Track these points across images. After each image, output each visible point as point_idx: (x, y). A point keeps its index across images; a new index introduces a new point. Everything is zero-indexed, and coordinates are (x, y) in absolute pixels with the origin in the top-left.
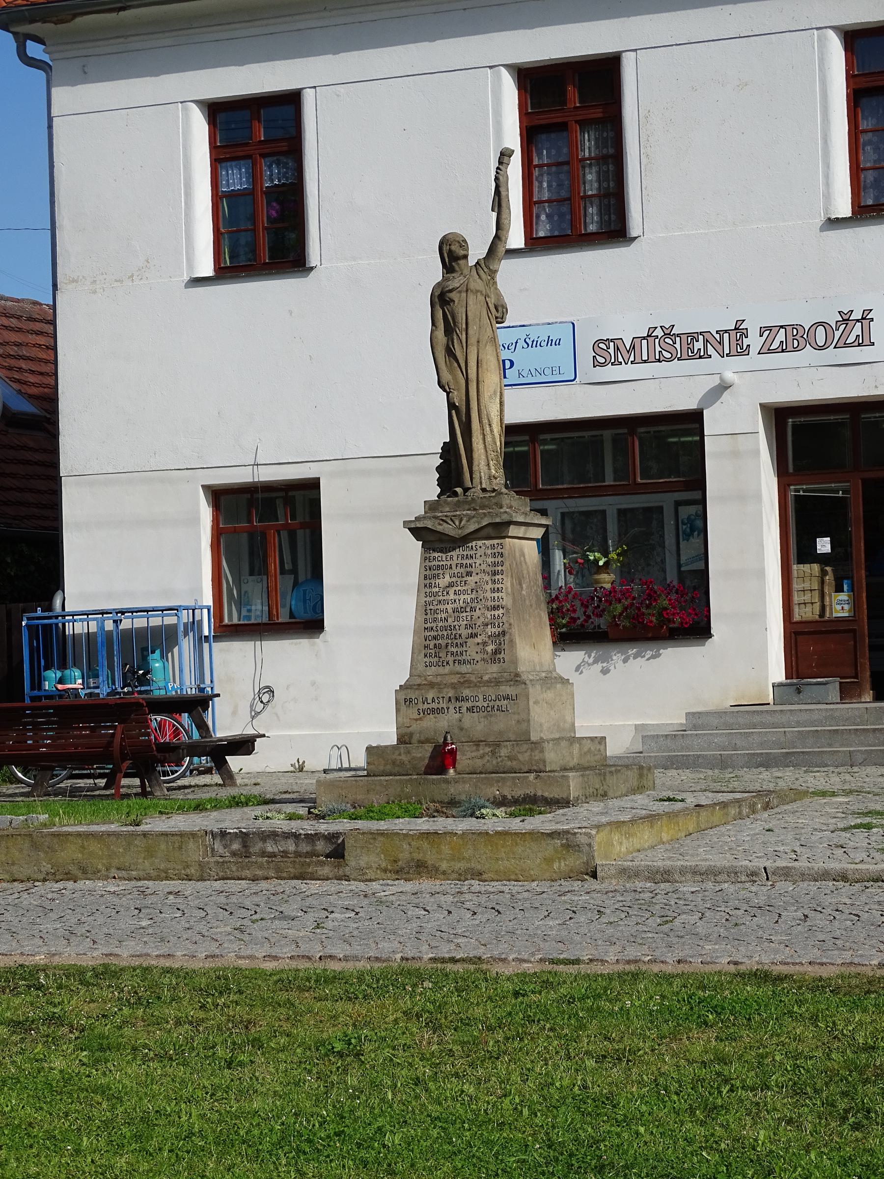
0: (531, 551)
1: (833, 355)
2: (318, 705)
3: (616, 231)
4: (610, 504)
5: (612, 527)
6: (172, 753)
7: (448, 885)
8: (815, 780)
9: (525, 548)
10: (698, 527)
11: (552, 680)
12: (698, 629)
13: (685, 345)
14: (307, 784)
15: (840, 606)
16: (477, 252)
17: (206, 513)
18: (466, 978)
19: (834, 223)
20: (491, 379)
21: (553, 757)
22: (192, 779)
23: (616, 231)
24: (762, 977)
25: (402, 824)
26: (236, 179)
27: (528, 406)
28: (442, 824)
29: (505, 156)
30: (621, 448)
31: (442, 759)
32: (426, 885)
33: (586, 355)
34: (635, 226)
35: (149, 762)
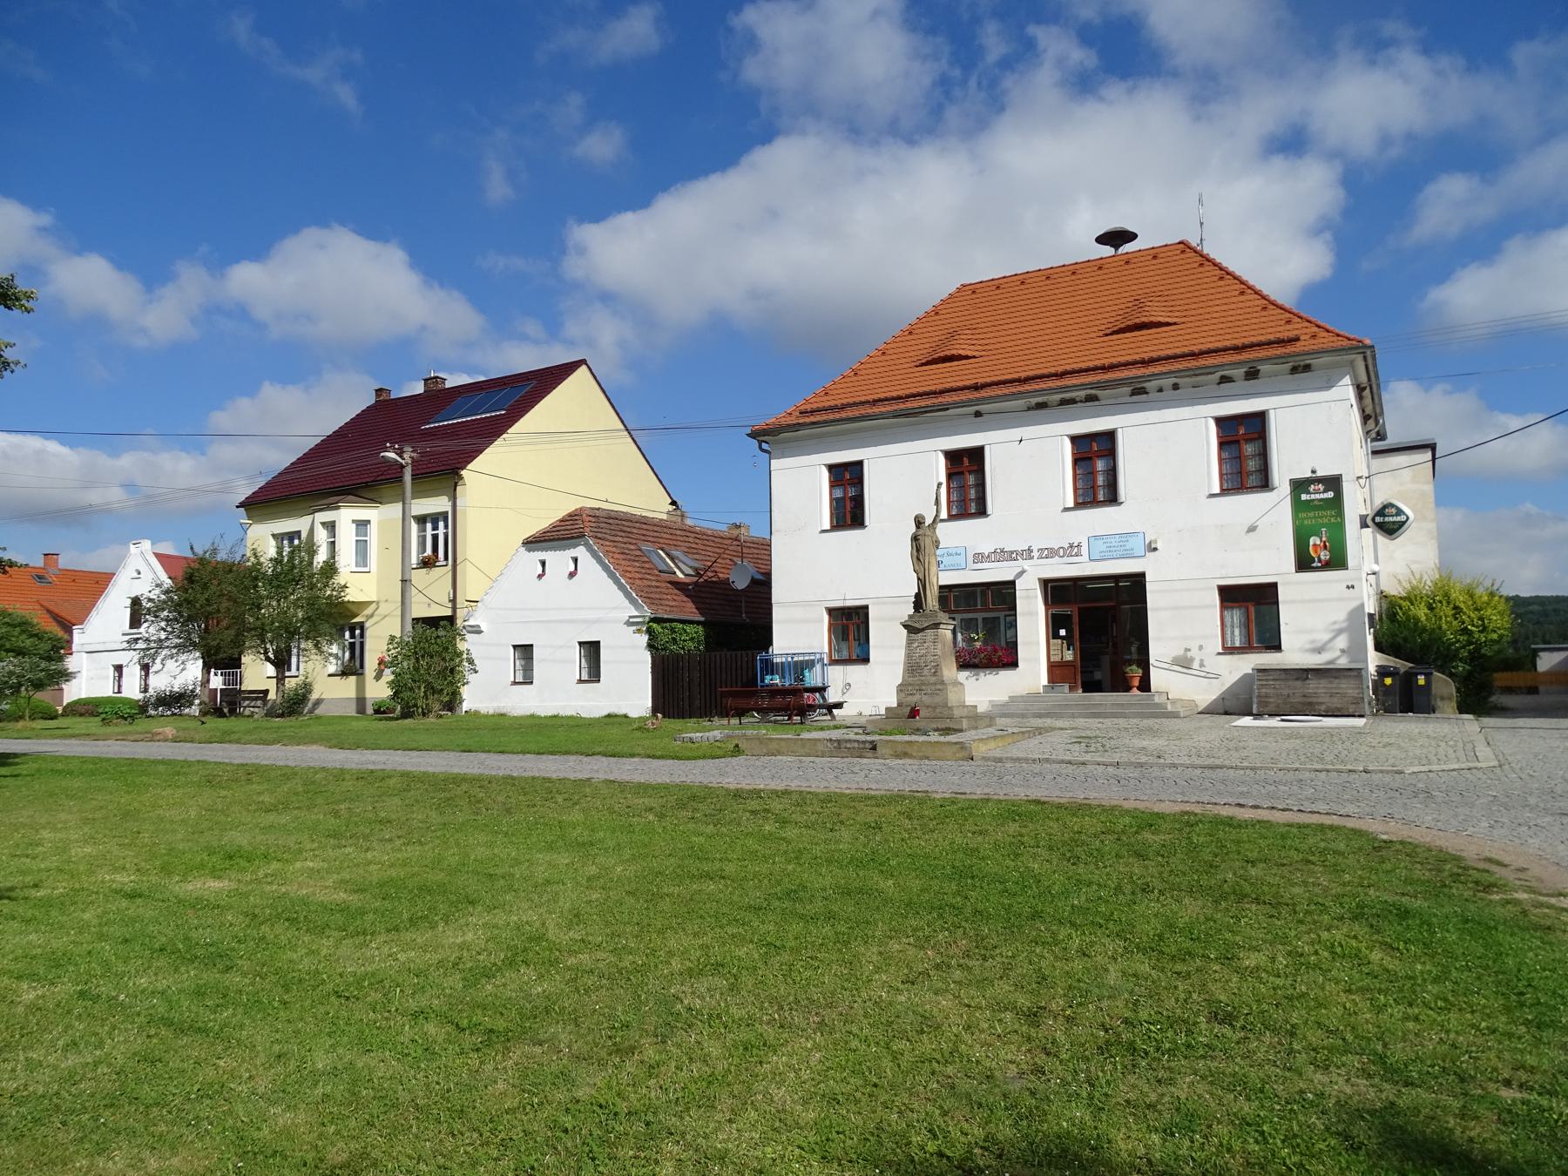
0: (949, 634)
1: (1066, 559)
2: (867, 691)
3: (982, 512)
4: (980, 616)
5: (980, 625)
6: (812, 708)
7: (916, 762)
8: (1059, 723)
9: (946, 633)
10: (1013, 625)
11: (957, 683)
12: (1014, 664)
13: (1011, 556)
14: (863, 721)
15: (1069, 656)
16: (928, 521)
17: (826, 617)
18: (923, 799)
19: (1066, 509)
20: (934, 569)
21: (956, 713)
22: (819, 717)
23: (982, 512)
24: (1037, 802)
25: (899, 738)
26: (839, 493)
27: (947, 578)
28: (913, 738)
29: (939, 485)
30: (984, 594)
31: (914, 713)
32: (908, 761)
33: (970, 559)
34: (989, 511)
35: (804, 711)
